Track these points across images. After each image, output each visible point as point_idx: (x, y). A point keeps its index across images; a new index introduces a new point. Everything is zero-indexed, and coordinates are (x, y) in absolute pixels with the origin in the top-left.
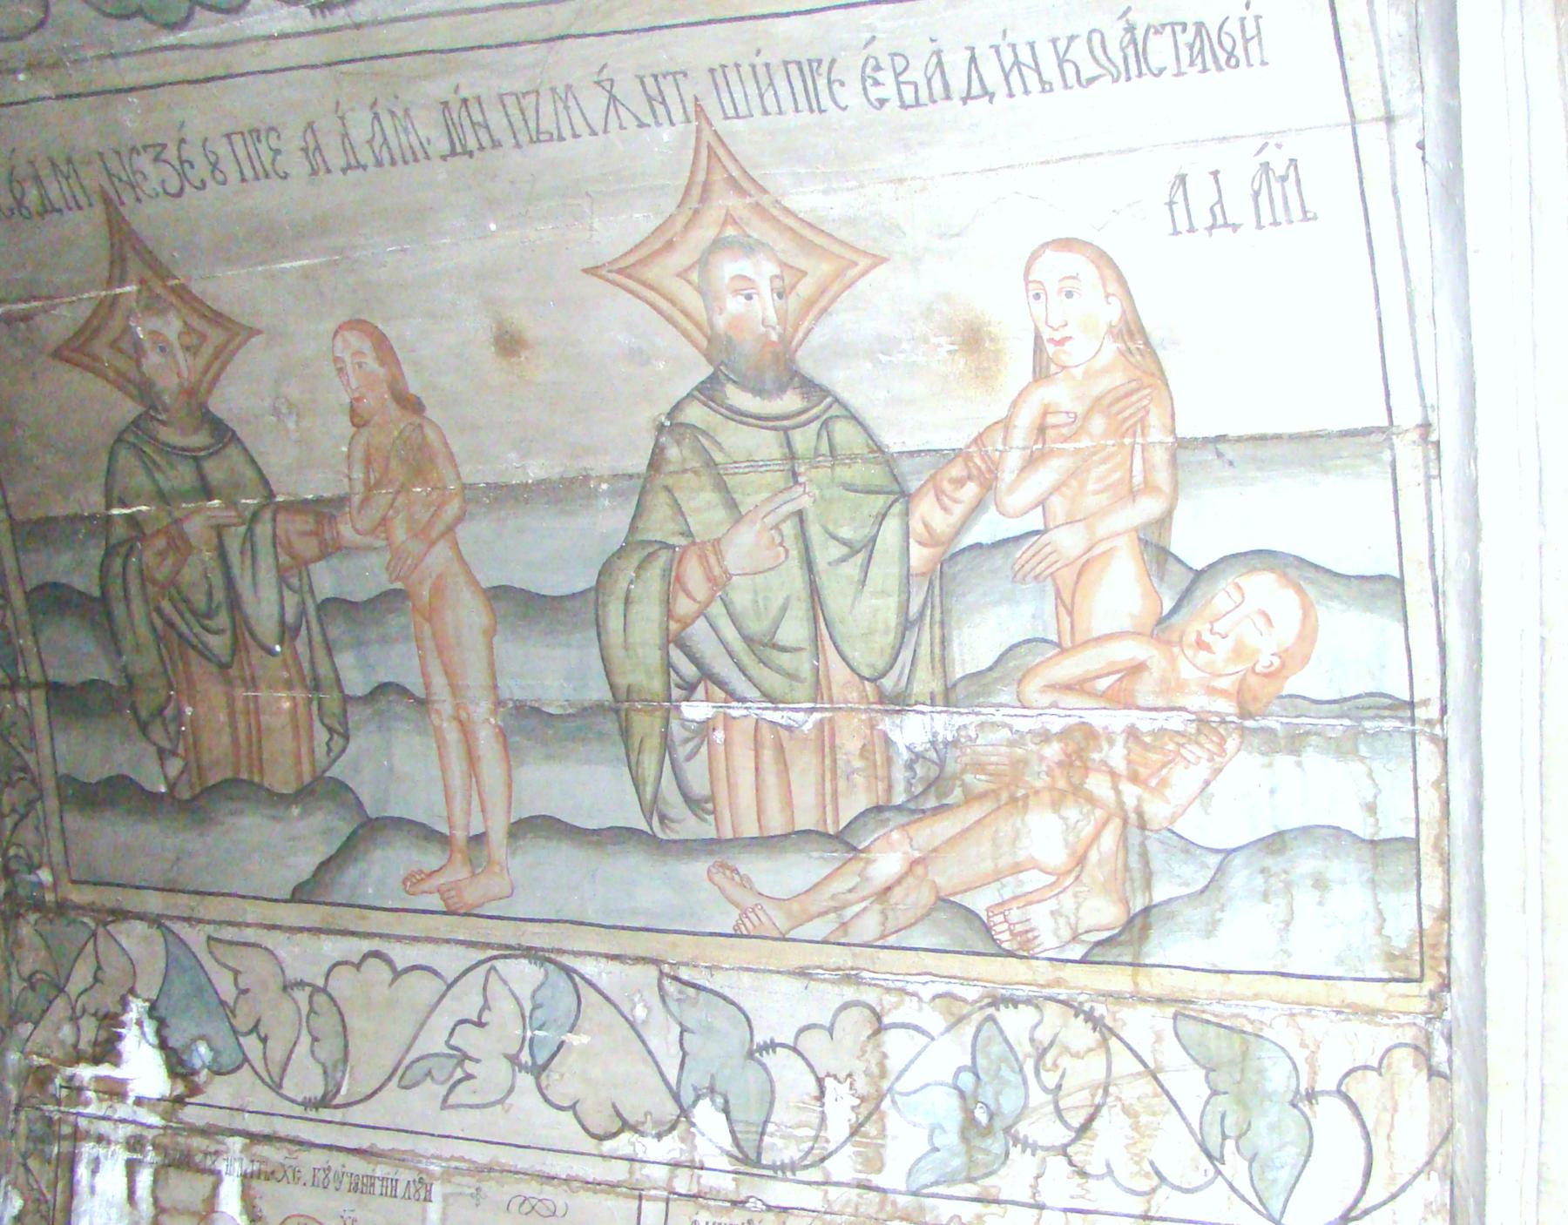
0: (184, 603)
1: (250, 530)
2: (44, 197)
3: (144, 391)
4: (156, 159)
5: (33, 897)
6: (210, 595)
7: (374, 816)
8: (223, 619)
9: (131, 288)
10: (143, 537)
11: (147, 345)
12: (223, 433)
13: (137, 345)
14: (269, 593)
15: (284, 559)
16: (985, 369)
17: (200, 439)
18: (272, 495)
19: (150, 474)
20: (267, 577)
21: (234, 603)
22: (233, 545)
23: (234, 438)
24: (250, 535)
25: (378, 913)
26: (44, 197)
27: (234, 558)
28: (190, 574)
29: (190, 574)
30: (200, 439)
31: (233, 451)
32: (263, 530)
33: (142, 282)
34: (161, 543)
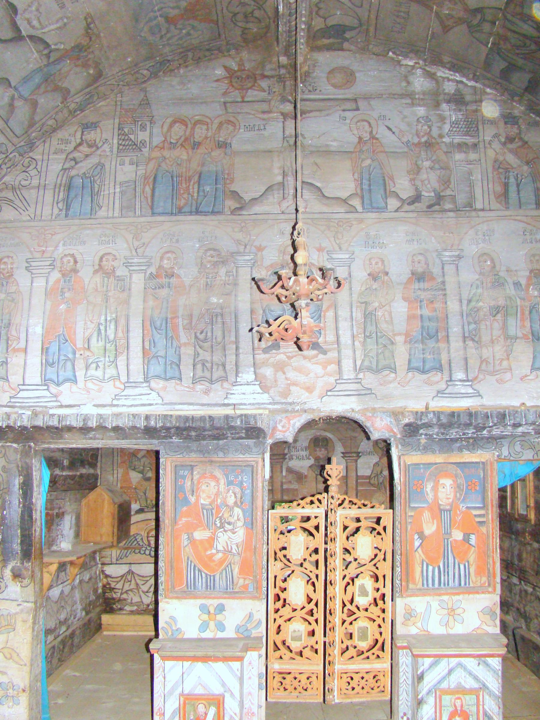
0: (518, 47)
1: (507, 19)
2: (404, 12)
3: (461, 21)
4: (3, 362)
5: (416, 423)
6: (520, 40)
7: (406, 304)
8: (528, 42)
9: (435, 7)
10: (499, 44)
11: (451, 12)
12: (479, 10)
13: (449, 15)
14: (526, 27)
15: (518, 17)
16: (63, 293)
17: (479, 16)
18: (501, 9)
19: (483, 32)
20: (521, 24)
21: (525, 36)
22: (509, 25)
23: (482, 8)
24: (509, 20)
25: (265, 604)
26: (404, 12)
27: (513, 28)
28: (513, 41)
29: (513, 41)
30: (479, 16)
31: (485, 11)
32: (509, 16)
33: (434, 4)
34: (502, 42)
